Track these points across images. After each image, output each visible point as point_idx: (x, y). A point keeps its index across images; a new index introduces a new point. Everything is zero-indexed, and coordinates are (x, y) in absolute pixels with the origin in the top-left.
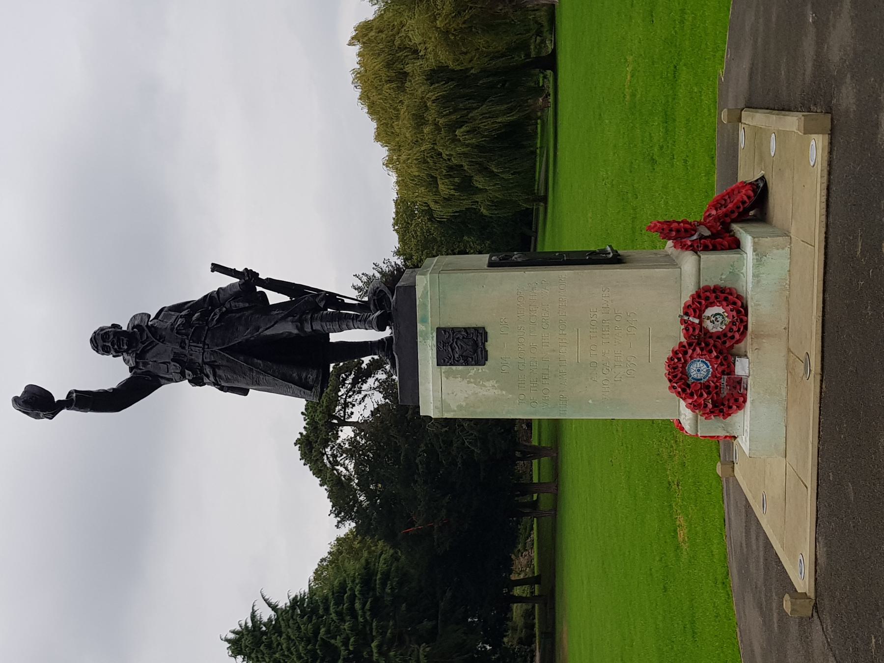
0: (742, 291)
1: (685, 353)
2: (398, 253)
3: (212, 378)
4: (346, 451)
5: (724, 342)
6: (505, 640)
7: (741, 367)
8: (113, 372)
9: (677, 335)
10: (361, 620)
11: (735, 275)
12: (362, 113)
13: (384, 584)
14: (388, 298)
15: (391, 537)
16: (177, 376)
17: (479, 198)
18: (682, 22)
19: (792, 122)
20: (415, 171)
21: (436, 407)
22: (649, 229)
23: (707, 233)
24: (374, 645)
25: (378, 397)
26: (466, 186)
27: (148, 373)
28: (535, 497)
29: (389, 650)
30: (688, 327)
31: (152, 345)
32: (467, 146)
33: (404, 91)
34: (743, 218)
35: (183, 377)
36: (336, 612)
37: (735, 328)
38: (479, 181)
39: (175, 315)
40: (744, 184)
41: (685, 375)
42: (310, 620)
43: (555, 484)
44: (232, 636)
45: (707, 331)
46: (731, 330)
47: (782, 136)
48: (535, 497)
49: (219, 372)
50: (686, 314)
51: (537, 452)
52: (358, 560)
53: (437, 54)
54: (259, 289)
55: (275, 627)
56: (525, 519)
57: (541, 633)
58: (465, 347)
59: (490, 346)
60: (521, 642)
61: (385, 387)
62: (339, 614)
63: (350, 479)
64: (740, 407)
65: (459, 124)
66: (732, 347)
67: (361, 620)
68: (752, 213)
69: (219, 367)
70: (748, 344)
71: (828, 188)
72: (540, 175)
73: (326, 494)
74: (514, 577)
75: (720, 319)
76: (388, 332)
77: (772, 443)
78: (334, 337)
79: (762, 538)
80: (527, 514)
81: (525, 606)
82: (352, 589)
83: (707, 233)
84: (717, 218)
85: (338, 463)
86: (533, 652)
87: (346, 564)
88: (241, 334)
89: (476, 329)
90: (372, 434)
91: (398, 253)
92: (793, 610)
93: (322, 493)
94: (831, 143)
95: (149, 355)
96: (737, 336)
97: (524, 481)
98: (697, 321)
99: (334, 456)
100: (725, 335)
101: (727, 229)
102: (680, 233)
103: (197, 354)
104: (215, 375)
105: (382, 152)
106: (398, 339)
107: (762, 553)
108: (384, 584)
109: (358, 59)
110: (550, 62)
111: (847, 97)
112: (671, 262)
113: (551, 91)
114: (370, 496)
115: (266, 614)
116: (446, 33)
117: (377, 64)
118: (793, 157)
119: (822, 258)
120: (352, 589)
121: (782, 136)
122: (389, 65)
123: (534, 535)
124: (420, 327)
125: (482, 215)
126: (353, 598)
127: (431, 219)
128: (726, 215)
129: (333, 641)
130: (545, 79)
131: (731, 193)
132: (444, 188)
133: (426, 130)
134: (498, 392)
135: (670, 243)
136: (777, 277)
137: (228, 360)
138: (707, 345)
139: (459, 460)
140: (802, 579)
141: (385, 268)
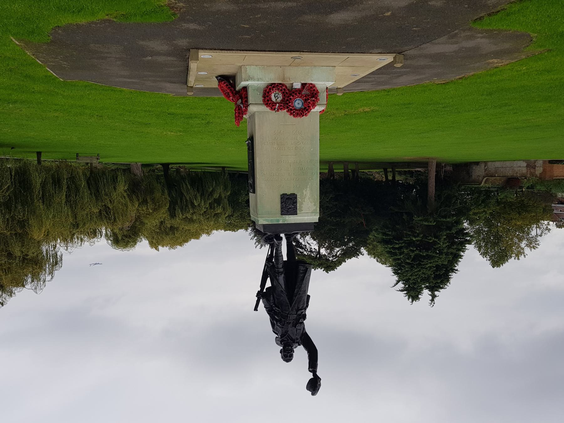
0: (265, 86)
1: (291, 110)
2: (247, 230)
3: (303, 311)
4: (331, 251)
5: (287, 93)
6: (411, 183)
7: (297, 86)
8: (300, 352)
9: (284, 113)
10: (403, 245)
11: (257, 89)
12: (187, 245)
13: (388, 235)
14: (268, 235)
15: (367, 232)
16: (302, 326)
17: (223, 196)
18: (150, 111)
19: (193, 65)
20: (212, 223)
22: (238, 125)
23: (240, 101)
24: (414, 239)
25: (308, 238)
26: (218, 201)
27: (301, 338)
28: (350, 171)
29: (416, 233)
30: (280, 108)
31: (289, 336)
32: (201, 201)
33: (178, 227)
34: (234, 85)
35: (302, 323)
36: (400, 255)
37: (281, 88)
38: (216, 196)
39: (276, 326)
41: (300, 109)
43: (345, 163)
44: (410, 300)
45: (282, 100)
46: (281, 90)
47: (199, 69)
48: (350, 171)
49: (300, 308)
50: (274, 109)
51: (331, 170)
52: (377, 246)
53: (163, 213)
54: (265, 291)
55: (406, 282)
56: (359, 175)
57: (408, 168)
58: (289, 203)
59: (289, 193)
60: (412, 177)
61: (303, 236)
62: (401, 254)
63: (343, 250)
64: (314, 86)
65: (192, 204)
66: (288, 90)
67: (403, 245)
68: (231, 82)
69: (298, 308)
70: (287, 83)
72: (214, 170)
73: (349, 260)
74: (384, 180)
75: (277, 95)
76: (282, 235)
77: (329, 72)
78: (285, 258)
79: (370, 76)
80: (357, 174)
81: (396, 175)
83: (240, 101)
84: (234, 96)
85: (336, 255)
87: (379, 251)
88: (284, 298)
89: (281, 199)
90: (324, 240)
91: (247, 230)
92: (401, 63)
93: (349, 261)
94: (202, 49)
95: (293, 338)
96: (284, 88)
98: (278, 105)
99: (333, 256)
100: (284, 93)
101: (238, 92)
102: (240, 113)
103: (293, 317)
104: (302, 309)
105: (204, 237)
106: (286, 232)
107: (376, 76)
108: (388, 235)
109: (165, 247)
110: (166, 166)
111: (183, 42)
112: (253, 116)
113: (178, 165)
116: (154, 210)
117: (167, 239)
118: (208, 65)
119: (251, 52)
120: (390, 249)
121: (199, 69)
122: (167, 234)
123: (366, 171)
124: (281, 222)
125: (230, 194)
126: (394, 248)
127: (232, 216)
128: (232, 93)
129: (412, 257)
130: (173, 168)
132: (219, 210)
133: (195, 218)
134: (308, 189)
135: (244, 116)
136: (257, 71)
137: (295, 304)
138: (287, 100)
139: (335, 203)
140: (388, 59)
141: (252, 235)
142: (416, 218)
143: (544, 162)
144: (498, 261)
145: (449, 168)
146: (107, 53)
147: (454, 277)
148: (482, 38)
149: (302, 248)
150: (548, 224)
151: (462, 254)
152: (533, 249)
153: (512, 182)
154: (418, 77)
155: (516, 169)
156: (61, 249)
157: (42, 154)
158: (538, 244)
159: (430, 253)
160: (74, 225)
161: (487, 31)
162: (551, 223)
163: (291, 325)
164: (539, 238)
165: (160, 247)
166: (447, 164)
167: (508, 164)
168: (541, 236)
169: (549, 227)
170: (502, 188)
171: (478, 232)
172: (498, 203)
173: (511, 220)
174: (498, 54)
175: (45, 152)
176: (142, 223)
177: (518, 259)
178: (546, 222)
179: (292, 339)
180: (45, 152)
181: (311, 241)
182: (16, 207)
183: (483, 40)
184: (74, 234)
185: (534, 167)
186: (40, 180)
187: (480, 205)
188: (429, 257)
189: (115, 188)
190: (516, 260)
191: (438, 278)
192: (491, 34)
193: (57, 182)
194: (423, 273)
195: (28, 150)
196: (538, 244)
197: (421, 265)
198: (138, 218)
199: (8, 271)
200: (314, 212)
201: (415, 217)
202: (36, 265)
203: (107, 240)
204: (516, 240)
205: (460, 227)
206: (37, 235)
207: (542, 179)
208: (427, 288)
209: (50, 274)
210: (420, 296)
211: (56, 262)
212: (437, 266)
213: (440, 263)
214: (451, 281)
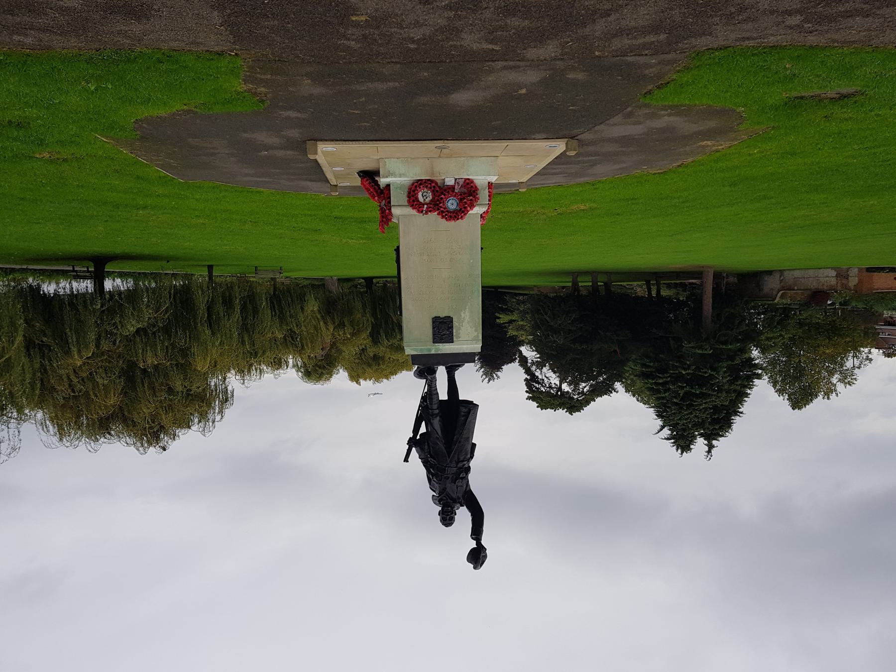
1: (443, 212)
7: (450, 182)
8: (463, 515)
9: (434, 216)
11: (401, 187)
14: (426, 370)
15: (623, 363)
16: (464, 481)
25: (545, 370)
31: (448, 495)
40: (362, 183)
42: (669, 407)
43: (593, 274)
44: (679, 451)
45: (431, 201)
49: (462, 458)
53: (364, 339)
54: (418, 437)
55: (673, 427)
57: (677, 279)
58: (443, 328)
59: (442, 315)
60: (684, 290)
66: (439, 187)
70: (438, 178)
73: (599, 398)
77: (488, 164)
82: (651, 384)
84: (378, 196)
86: (690, 284)
89: (433, 322)
93: (598, 400)
94: (321, 140)
97: (591, 289)
104: (463, 461)
110: (369, 280)
111: (294, 133)
114: (600, 374)
115: (666, 432)
116: (353, 335)
118: (339, 159)
120: (651, 384)
122: (369, 365)
123: (624, 284)
124: (433, 352)
126: (656, 384)
131: (368, 190)
140: (559, 147)
142: (686, 344)
143: (860, 270)
144: (799, 400)
145: (732, 279)
146: (213, 148)
147: (737, 421)
148: (669, 115)
149: (538, 383)
150: (870, 352)
151: (749, 391)
152: (848, 386)
153: (818, 296)
154: (617, 166)
155: (822, 280)
156: (233, 381)
157: (214, 268)
158: (855, 379)
159: (704, 390)
160: (251, 354)
161: (670, 107)
162: (873, 350)
163: (449, 481)
164: (856, 371)
165: (361, 381)
166: (729, 274)
167: (811, 273)
168: (859, 368)
169: (870, 356)
170: (806, 305)
171: (773, 363)
172: (801, 324)
173: (818, 346)
174: (708, 134)
175: (218, 266)
176: (340, 352)
177: (828, 398)
178: (866, 350)
179: (452, 499)
180: (218, 266)
181: (550, 374)
183: (672, 119)
184: (251, 365)
185: (847, 277)
186: (206, 299)
187: (776, 327)
188: (703, 396)
189: (302, 308)
190: (826, 399)
191: (717, 424)
192: (677, 110)
193: (228, 302)
194: (696, 416)
195: (191, 263)
196: (855, 379)
197: (693, 405)
198: (333, 345)
199: (170, 408)
200: (475, 339)
201: (681, 345)
202: (203, 401)
203: (297, 371)
204: (824, 374)
205: (747, 356)
206: (201, 365)
207: (858, 293)
208: (702, 435)
209: (219, 412)
210: (692, 447)
211: (226, 399)
212: (715, 408)
213: (718, 403)
214: (734, 426)
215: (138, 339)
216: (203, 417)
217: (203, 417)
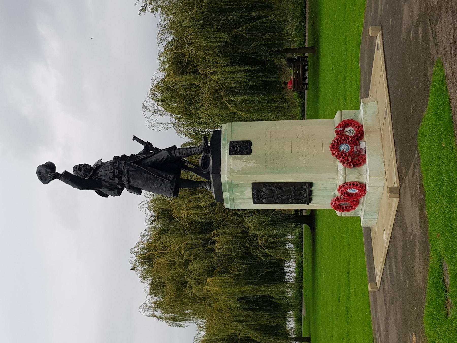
21: (228, 171)
59: (252, 148)
71: (383, 46)
75: (352, 132)
77: (378, 171)
124: (222, 142)
182: (244, 264)
215: (239, 230)
216: (158, 305)
217: (158, 305)
